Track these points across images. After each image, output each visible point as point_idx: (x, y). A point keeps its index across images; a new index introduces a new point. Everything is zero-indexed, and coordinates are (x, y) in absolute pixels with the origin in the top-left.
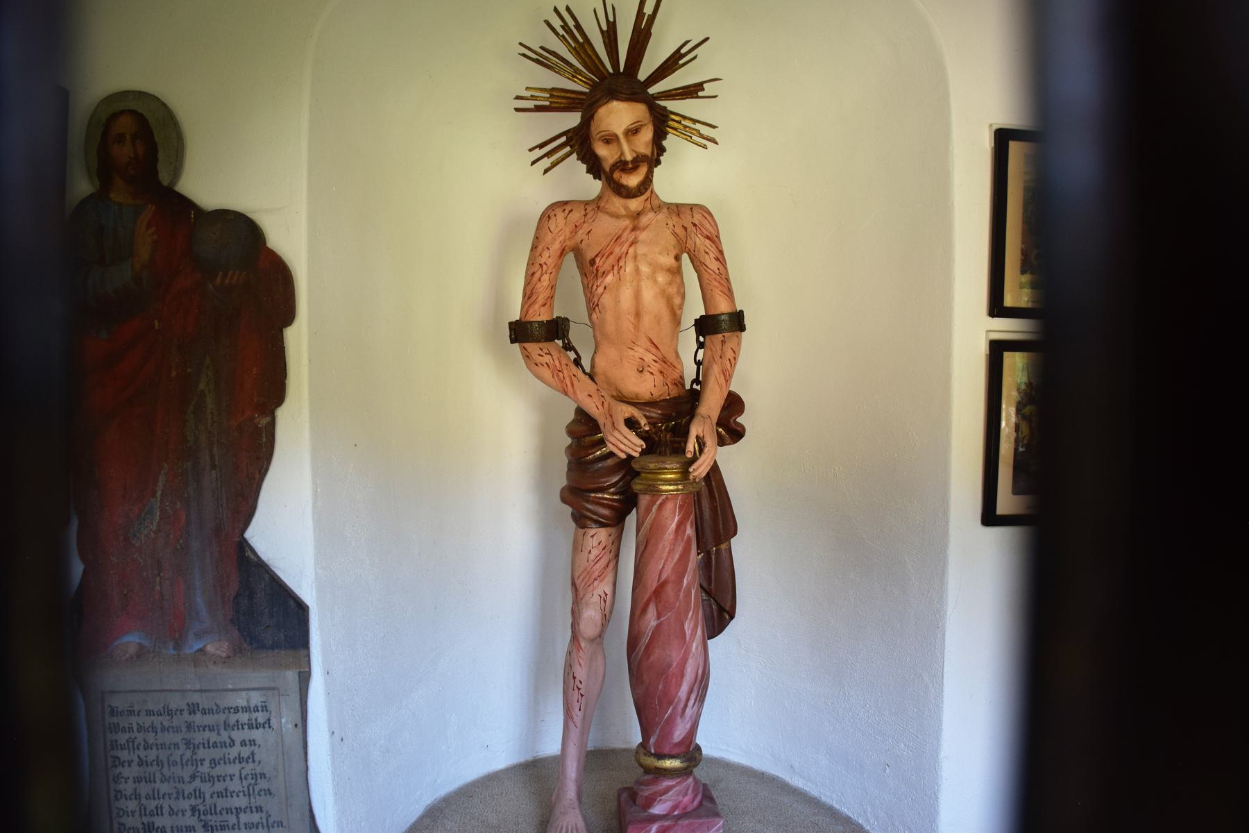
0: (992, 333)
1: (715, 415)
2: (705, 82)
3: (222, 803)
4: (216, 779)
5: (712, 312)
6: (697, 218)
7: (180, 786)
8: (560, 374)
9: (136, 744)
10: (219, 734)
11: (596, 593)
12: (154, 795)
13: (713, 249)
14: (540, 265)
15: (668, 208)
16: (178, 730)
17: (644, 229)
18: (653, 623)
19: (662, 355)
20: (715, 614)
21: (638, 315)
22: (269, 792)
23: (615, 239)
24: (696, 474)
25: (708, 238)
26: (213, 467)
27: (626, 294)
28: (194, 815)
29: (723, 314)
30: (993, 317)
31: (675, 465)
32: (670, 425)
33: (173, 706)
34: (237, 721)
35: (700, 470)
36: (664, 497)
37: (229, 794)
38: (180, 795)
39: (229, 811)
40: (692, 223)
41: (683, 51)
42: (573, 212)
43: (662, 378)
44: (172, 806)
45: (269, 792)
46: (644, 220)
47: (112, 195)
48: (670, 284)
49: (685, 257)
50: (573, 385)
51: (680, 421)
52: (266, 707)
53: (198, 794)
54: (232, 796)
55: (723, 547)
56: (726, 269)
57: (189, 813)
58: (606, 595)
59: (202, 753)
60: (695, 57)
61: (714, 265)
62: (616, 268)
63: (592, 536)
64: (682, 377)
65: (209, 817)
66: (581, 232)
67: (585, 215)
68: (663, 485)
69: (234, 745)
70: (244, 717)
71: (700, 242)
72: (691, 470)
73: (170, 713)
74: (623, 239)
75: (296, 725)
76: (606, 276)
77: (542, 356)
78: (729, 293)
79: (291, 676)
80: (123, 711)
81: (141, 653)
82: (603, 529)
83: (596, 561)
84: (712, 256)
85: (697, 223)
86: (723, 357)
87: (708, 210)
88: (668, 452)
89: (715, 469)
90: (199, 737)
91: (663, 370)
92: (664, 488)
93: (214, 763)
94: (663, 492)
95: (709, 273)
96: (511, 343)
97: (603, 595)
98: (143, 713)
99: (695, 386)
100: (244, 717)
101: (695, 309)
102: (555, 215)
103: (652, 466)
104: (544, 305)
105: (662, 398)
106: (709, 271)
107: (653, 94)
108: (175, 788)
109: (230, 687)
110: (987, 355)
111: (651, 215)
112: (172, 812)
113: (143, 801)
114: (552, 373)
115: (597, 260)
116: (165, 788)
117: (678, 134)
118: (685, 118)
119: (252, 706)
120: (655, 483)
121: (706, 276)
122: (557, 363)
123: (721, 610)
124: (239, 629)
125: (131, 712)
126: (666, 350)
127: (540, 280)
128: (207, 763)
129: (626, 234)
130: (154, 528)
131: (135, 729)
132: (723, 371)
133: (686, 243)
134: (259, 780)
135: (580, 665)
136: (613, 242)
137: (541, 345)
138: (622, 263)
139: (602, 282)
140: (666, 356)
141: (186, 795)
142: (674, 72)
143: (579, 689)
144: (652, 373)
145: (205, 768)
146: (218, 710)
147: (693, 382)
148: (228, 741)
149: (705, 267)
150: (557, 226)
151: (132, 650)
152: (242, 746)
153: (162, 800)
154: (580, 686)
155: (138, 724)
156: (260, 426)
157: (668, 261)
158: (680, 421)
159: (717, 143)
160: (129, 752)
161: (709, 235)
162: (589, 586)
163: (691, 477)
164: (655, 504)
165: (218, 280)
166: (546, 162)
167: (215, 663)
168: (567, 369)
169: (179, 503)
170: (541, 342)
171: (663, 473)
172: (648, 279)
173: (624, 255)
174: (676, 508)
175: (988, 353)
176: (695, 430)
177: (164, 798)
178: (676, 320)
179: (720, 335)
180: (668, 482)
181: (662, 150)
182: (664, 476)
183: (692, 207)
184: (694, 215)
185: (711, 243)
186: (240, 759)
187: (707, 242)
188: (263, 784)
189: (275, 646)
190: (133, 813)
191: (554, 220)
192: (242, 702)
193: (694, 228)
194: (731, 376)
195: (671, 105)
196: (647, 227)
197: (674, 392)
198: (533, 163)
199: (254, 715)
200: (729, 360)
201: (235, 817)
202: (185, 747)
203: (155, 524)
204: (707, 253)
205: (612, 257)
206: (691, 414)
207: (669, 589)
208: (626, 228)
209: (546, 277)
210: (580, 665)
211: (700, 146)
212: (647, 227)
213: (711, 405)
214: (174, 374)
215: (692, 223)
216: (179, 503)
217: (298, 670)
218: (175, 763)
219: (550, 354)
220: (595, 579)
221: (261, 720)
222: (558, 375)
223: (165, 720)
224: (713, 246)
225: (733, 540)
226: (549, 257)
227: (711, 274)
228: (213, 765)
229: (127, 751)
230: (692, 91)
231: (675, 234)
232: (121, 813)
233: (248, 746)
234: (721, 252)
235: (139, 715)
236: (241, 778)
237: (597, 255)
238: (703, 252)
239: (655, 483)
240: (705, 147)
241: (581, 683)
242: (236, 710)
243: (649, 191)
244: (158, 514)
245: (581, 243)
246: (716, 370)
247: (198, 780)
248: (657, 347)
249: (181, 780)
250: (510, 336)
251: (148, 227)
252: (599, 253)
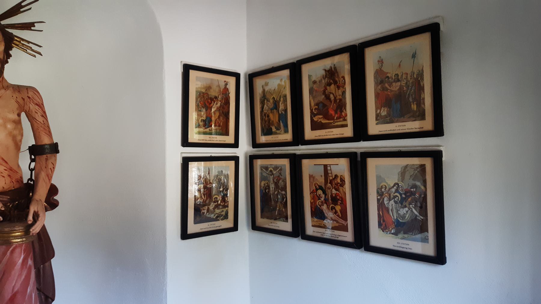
0: (184, 154)
1: (43, 199)
2: (36, 22)
5: (39, 144)
6: (31, 94)
13: (40, 110)
15: (13, 88)
19: (10, 166)
20: (43, 300)
24: (34, 232)
25: (37, 105)
29: (47, 145)
30: (184, 147)
31: (21, 228)
32: (15, 203)
35: (36, 229)
36: (14, 246)
40: (28, 96)
41: (23, 4)
43: (10, 179)
48: (15, 129)
49: (23, 115)
51: (21, 201)
55: (47, 264)
56: (47, 121)
60: (30, 9)
61: (40, 119)
64: (21, 178)
68: (14, 239)
71: (33, 107)
72: (31, 230)
78: (50, 134)
84: (39, 114)
85: (30, 96)
86: (47, 167)
87: (37, 90)
88: (16, 220)
89: (44, 228)
91: (10, 175)
94: (14, 243)
95: (37, 123)
99: (29, 182)
101: (29, 140)
103: (6, 229)
105: (9, 190)
106: (37, 122)
107: (4, 25)
110: (181, 163)
117: (19, 48)
118: (23, 40)
120: (8, 239)
121: (36, 125)
123: (47, 297)
126: (12, 164)
132: (47, 174)
133: (24, 107)
140: (12, 167)
142: (17, 14)
144: (3, 177)
147: (28, 180)
149: (35, 120)
157: (14, 116)
158: (21, 201)
159: (42, 55)
161: (38, 103)
163: (31, 234)
164: (9, 250)
174: (21, 251)
175: (182, 163)
176: (33, 209)
178: (18, 148)
179: (45, 156)
180: (17, 237)
181: (9, 56)
182: (14, 234)
183: (28, 88)
184: (29, 92)
185: (39, 108)
187: (37, 107)
193: (29, 100)
194: (51, 177)
195: (16, 32)
197: (17, 186)
200: (51, 168)
204: (37, 113)
206: (29, 201)
207: (19, 297)
211: (29, 54)
213: (41, 193)
215: (28, 96)
224: (40, 109)
225: (52, 260)
227: (38, 124)
230: (28, 26)
231: (17, 102)
234: (45, 112)
238: (34, 113)
239: (8, 239)
240: (35, 56)
243: (2, 78)
246: (43, 175)
248: (6, 162)
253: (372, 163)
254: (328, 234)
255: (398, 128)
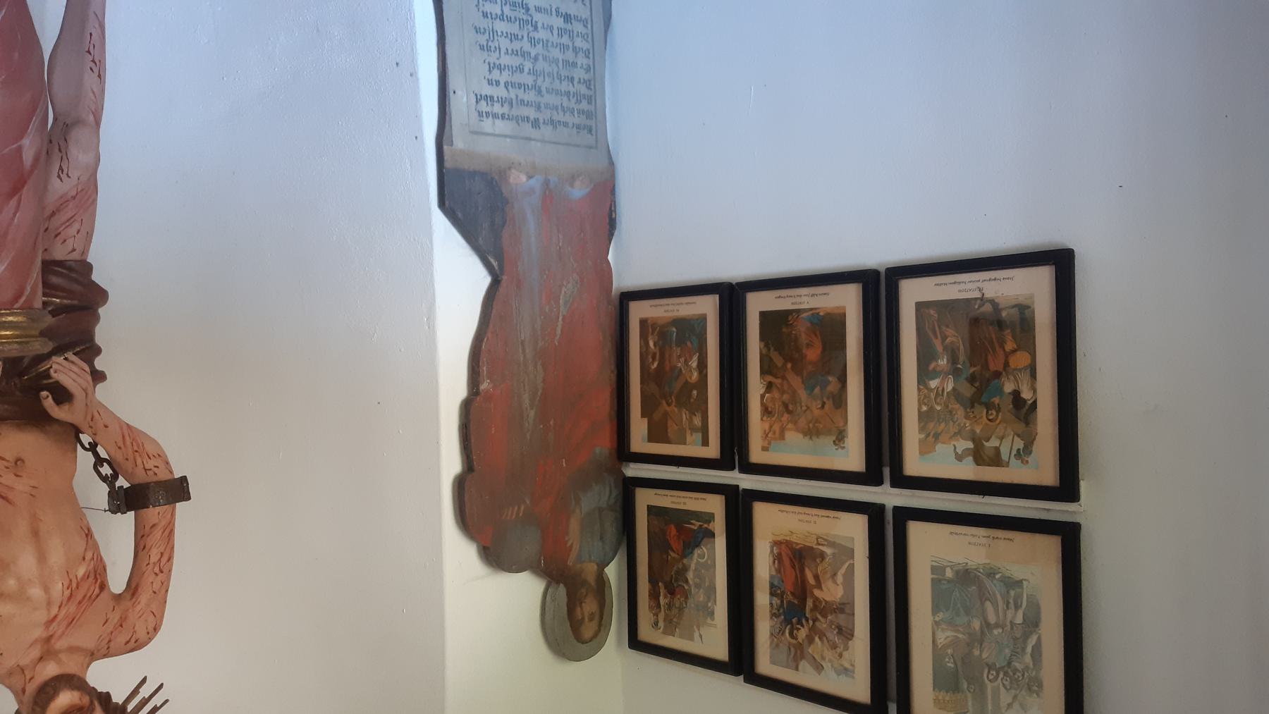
3: (514, 28)
4: (519, 53)
7: (545, 53)
8: (136, 448)
9: (575, 98)
10: (517, 96)
11: (74, 181)
12: (564, 48)
14: (162, 572)
16: (547, 106)
17: (36, 641)
18: (26, 142)
21: (36, 533)
22: (477, 30)
23: (75, 620)
26: (523, 342)
27: (57, 557)
28: (536, 22)
33: (550, 128)
34: (502, 106)
36: (17, 306)
37: (509, 36)
38: (546, 44)
39: (509, 20)
42: (124, 642)
44: (551, 34)
45: (477, 30)
46: (36, 653)
47: (596, 567)
50: (123, 437)
52: (479, 115)
53: (533, 42)
54: (507, 33)
57: (540, 25)
58: (59, 176)
59: (529, 80)
62: (74, 585)
63: (74, 250)
65: (525, 17)
66: (116, 620)
67: (110, 641)
68: (21, 322)
69: (505, 84)
70: (497, 108)
73: (552, 122)
74: (65, 623)
75: (454, 92)
76: (85, 573)
77: (155, 467)
79: (460, 141)
80: (584, 129)
81: (573, 178)
82: (57, 259)
83: (72, 220)
90: (530, 96)
92: (20, 319)
93: (520, 69)
96: (185, 477)
97: (64, 176)
98: (571, 125)
100: (497, 108)
102: (148, 633)
104: (154, 526)
108: (549, 51)
109: (508, 140)
111: (25, 661)
112: (551, 28)
113: (571, 45)
114: (144, 448)
115: (97, 591)
116: (556, 53)
119: (491, 118)
122: (139, 461)
124: (502, 194)
125: (578, 127)
127: (162, 554)
128: (526, 70)
129: (59, 632)
130: (564, 289)
131: (576, 112)
134: (485, 44)
135: (93, 93)
136: (77, 617)
137: (155, 479)
138: (67, 593)
139: (89, 565)
141: (541, 43)
143: (93, 61)
145: (528, 65)
146: (520, 120)
148: (510, 87)
150: (146, 621)
151: (577, 183)
152: (499, 81)
153: (558, 42)
154: (92, 65)
155: (574, 115)
156: (488, 381)
160: (580, 92)
162: (82, 190)
165: (522, 508)
166: (145, 692)
167: (520, 164)
168: (127, 455)
169: (547, 310)
170: (155, 482)
171: (17, 337)
172: (30, 580)
173: (64, 603)
177: (557, 43)
186: (500, 68)
188: (483, 39)
189: (473, 174)
190: (578, 36)
191: (149, 627)
192: (499, 122)
196: (30, 646)
198: (161, 686)
199: (489, 109)
201: (505, 12)
202: (542, 88)
203: (563, 292)
205: (79, 597)
208: (60, 637)
209: (154, 558)
210: (93, 93)
212: (30, 646)
214: (552, 423)
216: (547, 310)
217: (453, 147)
218: (549, 75)
219: (146, 470)
220: (74, 198)
221: (483, 103)
222: (138, 447)
223: (556, 117)
226: (152, 583)
228: (521, 67)
229: (582, 93)
232: (586, 37)
233: (493, 80)
235: (573, 124)
236: (500, 49)
237: (98, 596)
241: (91, 69)
242: (503, 117)
244: (561, 301)
245: (114, 607)
247: (533, 55)
249: (545, 58)
250: (188, 484)
251: (572, 546)
252: (94, 600)
253: (917, 531)
254: (805, 299)
255: (682, 500)
